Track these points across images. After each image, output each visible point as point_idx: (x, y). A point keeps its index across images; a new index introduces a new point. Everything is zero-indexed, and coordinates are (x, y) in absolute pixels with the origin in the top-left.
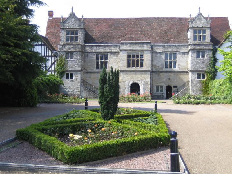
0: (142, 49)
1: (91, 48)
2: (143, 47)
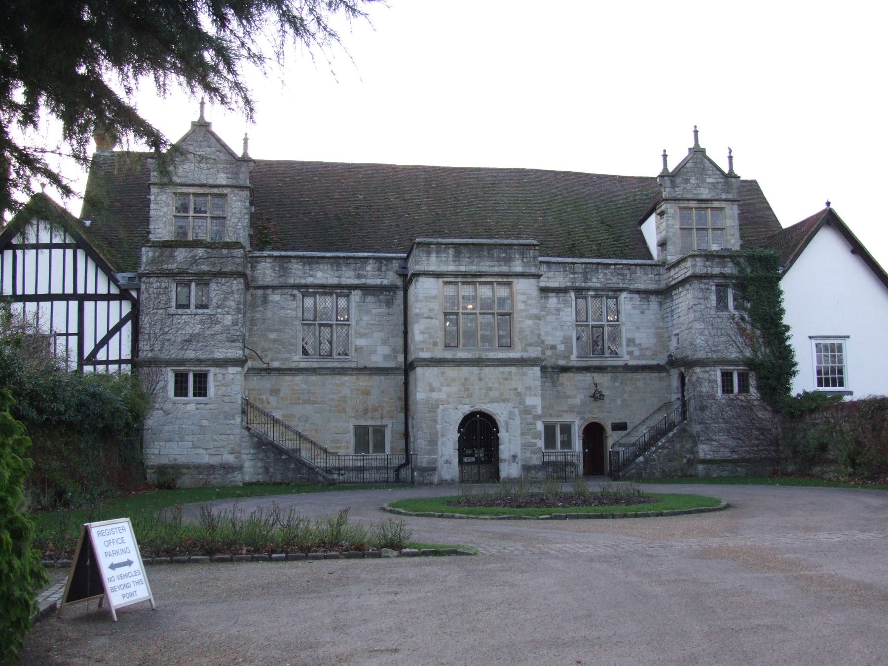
0: (504, 269)
1: (281, 267)
2: (508, 260)
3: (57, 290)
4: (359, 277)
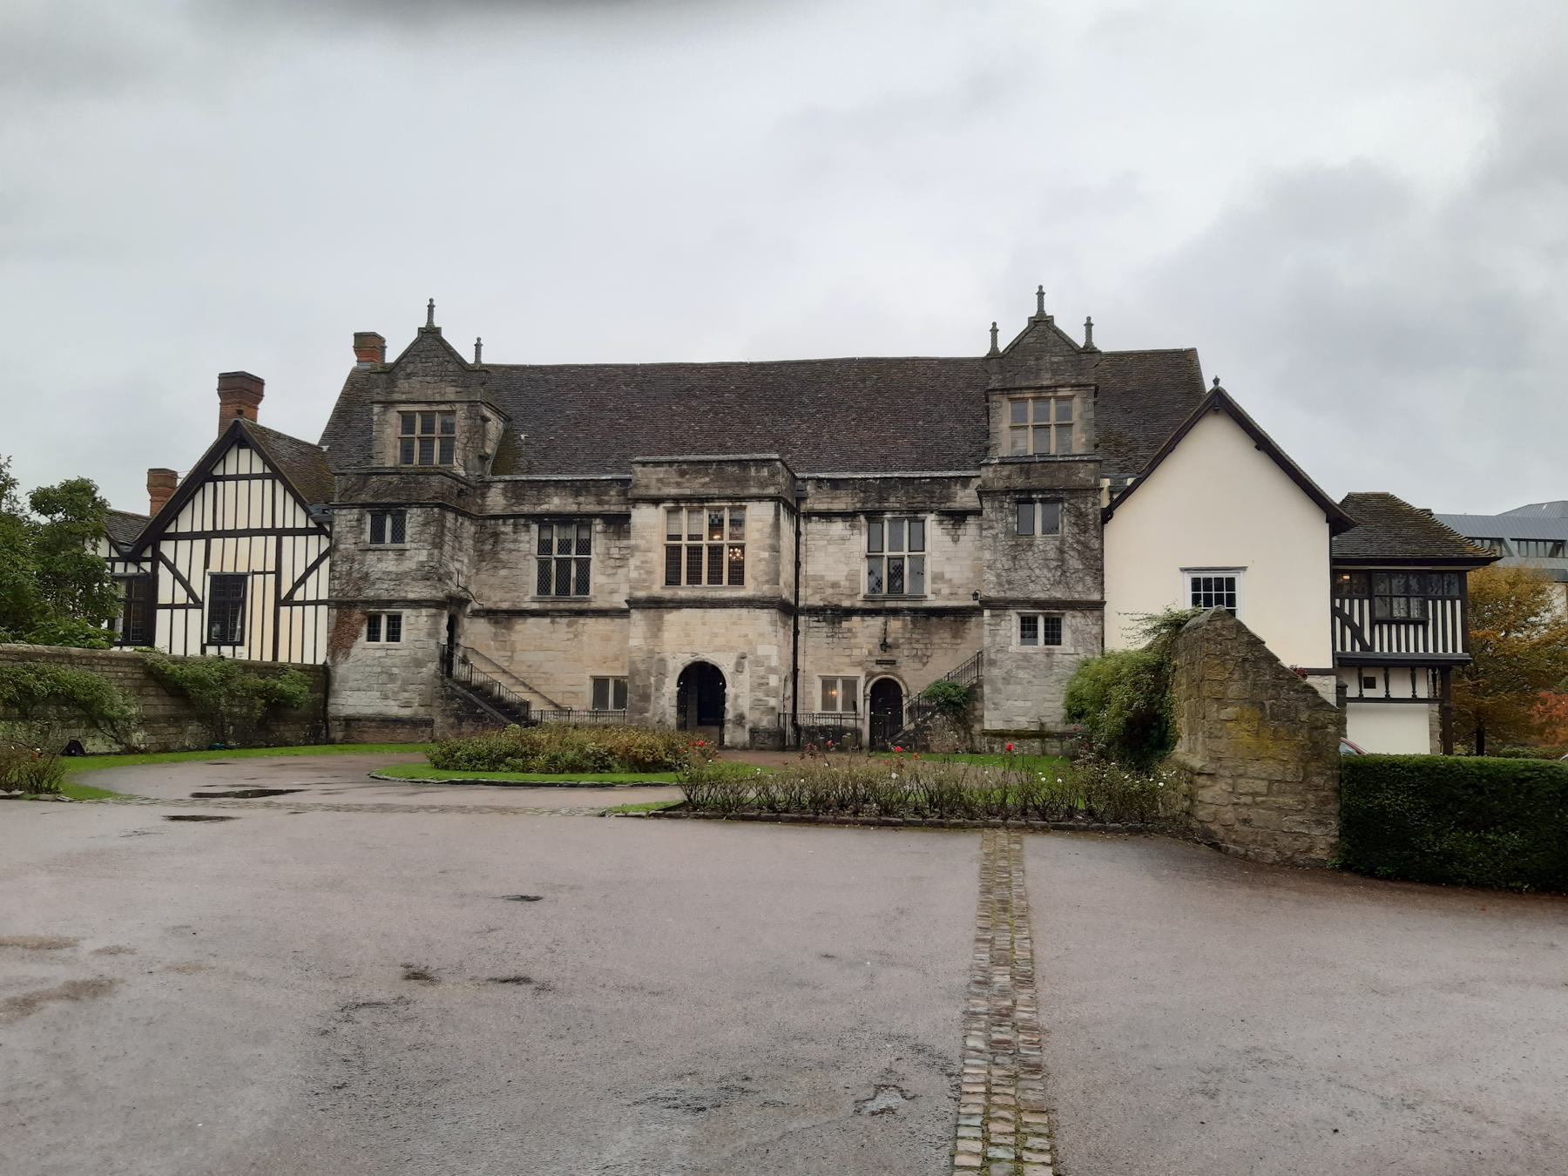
3: (255, 525)
4: (600, 503)
